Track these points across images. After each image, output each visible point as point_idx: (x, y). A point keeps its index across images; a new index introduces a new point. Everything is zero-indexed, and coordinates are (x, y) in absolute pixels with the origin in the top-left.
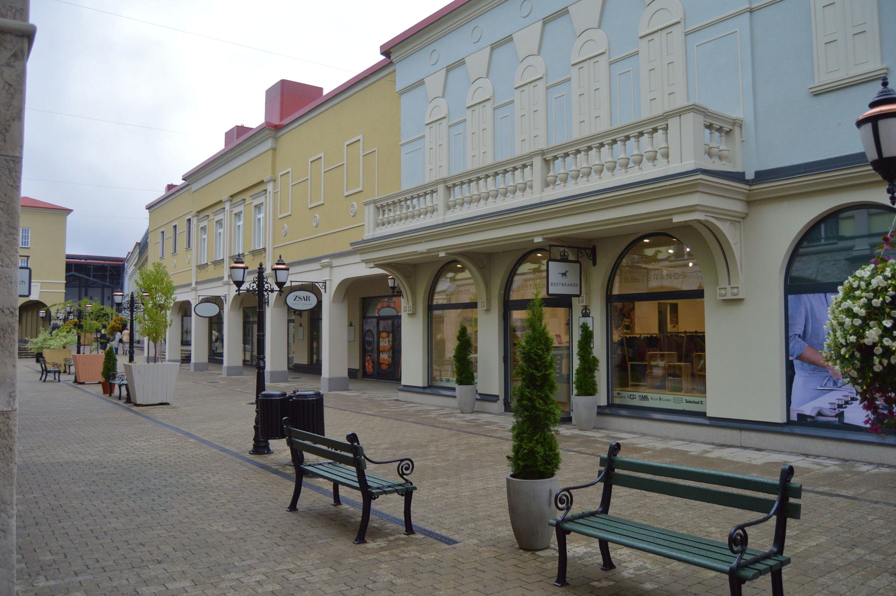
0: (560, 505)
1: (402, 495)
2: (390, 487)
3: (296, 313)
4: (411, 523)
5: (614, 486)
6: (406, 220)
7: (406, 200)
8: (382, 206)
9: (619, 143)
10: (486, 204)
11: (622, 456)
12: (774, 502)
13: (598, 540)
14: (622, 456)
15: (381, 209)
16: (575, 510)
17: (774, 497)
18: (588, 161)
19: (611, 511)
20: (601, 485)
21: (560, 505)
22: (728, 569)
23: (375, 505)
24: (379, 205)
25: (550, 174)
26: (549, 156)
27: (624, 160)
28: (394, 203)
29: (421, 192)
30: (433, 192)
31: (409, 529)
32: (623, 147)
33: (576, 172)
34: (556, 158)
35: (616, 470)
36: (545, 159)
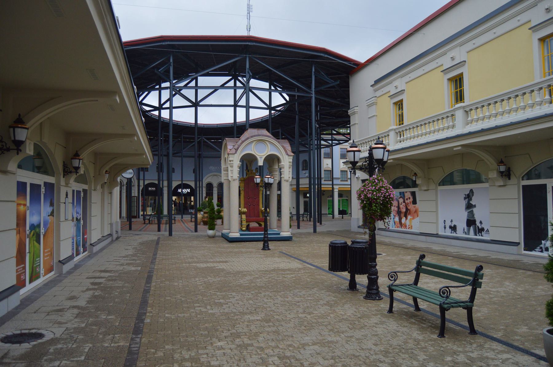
0: (391, 279)
1: (466, 309)
2: (455, 303)
3: (504, 174)
4: (474, 328)
5: (421, 274)
6: (453, 129)
7: (369, 141)
8: (400, 132)
9: (527, 94)
10: (532, 111)
11: (426, 260)
12: (471, 280)
13: (412, 297)
14: (426, 260)
15: (398, 134)
16: (397, 282)
17: (471, 278)
18: (438, 125)
19: (419, 285)
20: (414, 272)
21: (391, 279)
22: (439, 303)
23: (448, 314)
24: (397, 131)
25: (469, 119)
26: (468, 109)
27: (476, 119)
28: (364, 143)
29: (544, 85)
30: (453, 115)
31: (473, 331)
32: (494, 107)
33: (516, 109)
34: (471, 110)
35: (423, 267)
36: (465, 111)
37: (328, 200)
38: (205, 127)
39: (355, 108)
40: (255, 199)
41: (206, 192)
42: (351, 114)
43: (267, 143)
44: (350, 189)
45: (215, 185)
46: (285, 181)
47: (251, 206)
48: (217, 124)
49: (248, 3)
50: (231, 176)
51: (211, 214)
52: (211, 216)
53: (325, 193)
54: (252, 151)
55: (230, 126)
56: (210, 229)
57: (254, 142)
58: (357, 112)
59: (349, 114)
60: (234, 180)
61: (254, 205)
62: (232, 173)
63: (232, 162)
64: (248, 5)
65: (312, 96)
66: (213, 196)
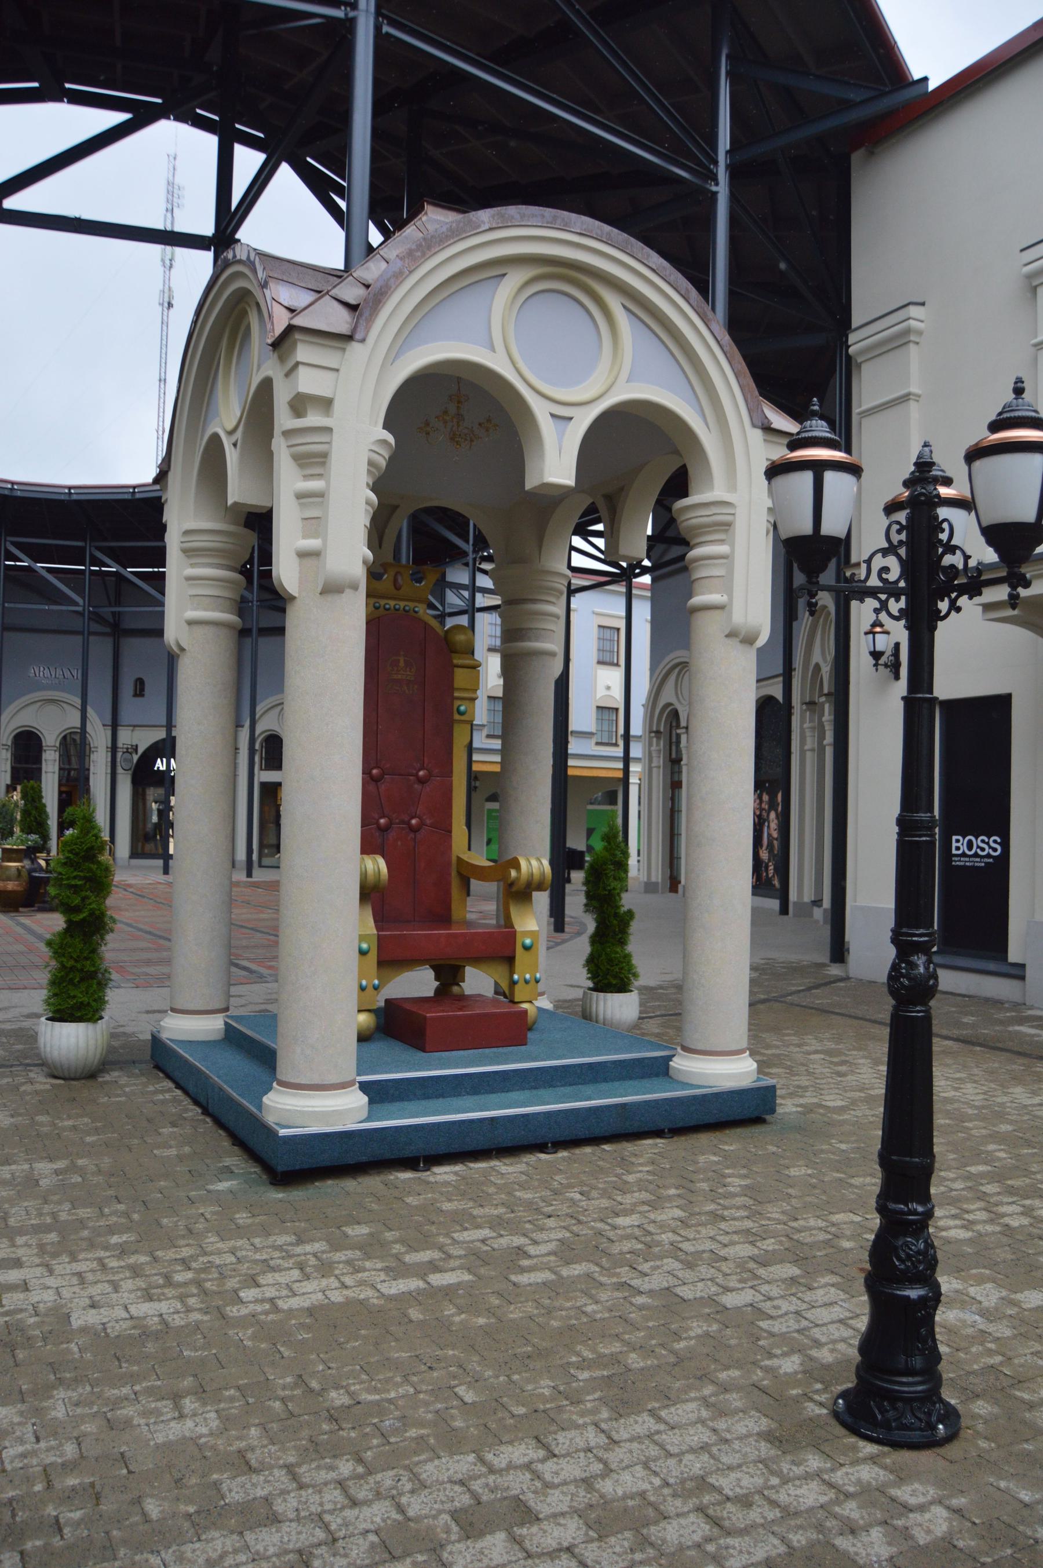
37: (489, 810)
38: (19, 494)
39: (913, 311)
40: (422, 781)
41: (13, 768)
42: (862, 352)
43: (614, 302)
44: (620, 775)
45: (51, 739)
46: (734, 642)
47: (392, 835)
48: (70, 488)
49: (171, 178)
50: (303, 555)
51: (76, 889)
52: (77, 910)
53: (478, 784)
54: (493, 349)
55: (126, 497)
56: (61, 1015)
57: (515, 278)
58: (920, 333)
59: (851, 350)
60: (332, 589)
61: (414, 830)
62: (314, 525)
63: (313, 419)
64: (170, 184)
65: (715, 193)
66: (40, 781)
